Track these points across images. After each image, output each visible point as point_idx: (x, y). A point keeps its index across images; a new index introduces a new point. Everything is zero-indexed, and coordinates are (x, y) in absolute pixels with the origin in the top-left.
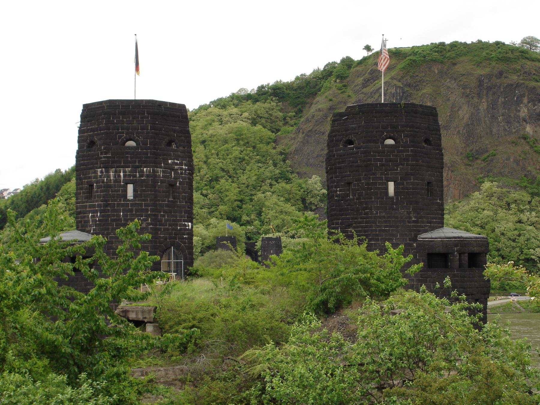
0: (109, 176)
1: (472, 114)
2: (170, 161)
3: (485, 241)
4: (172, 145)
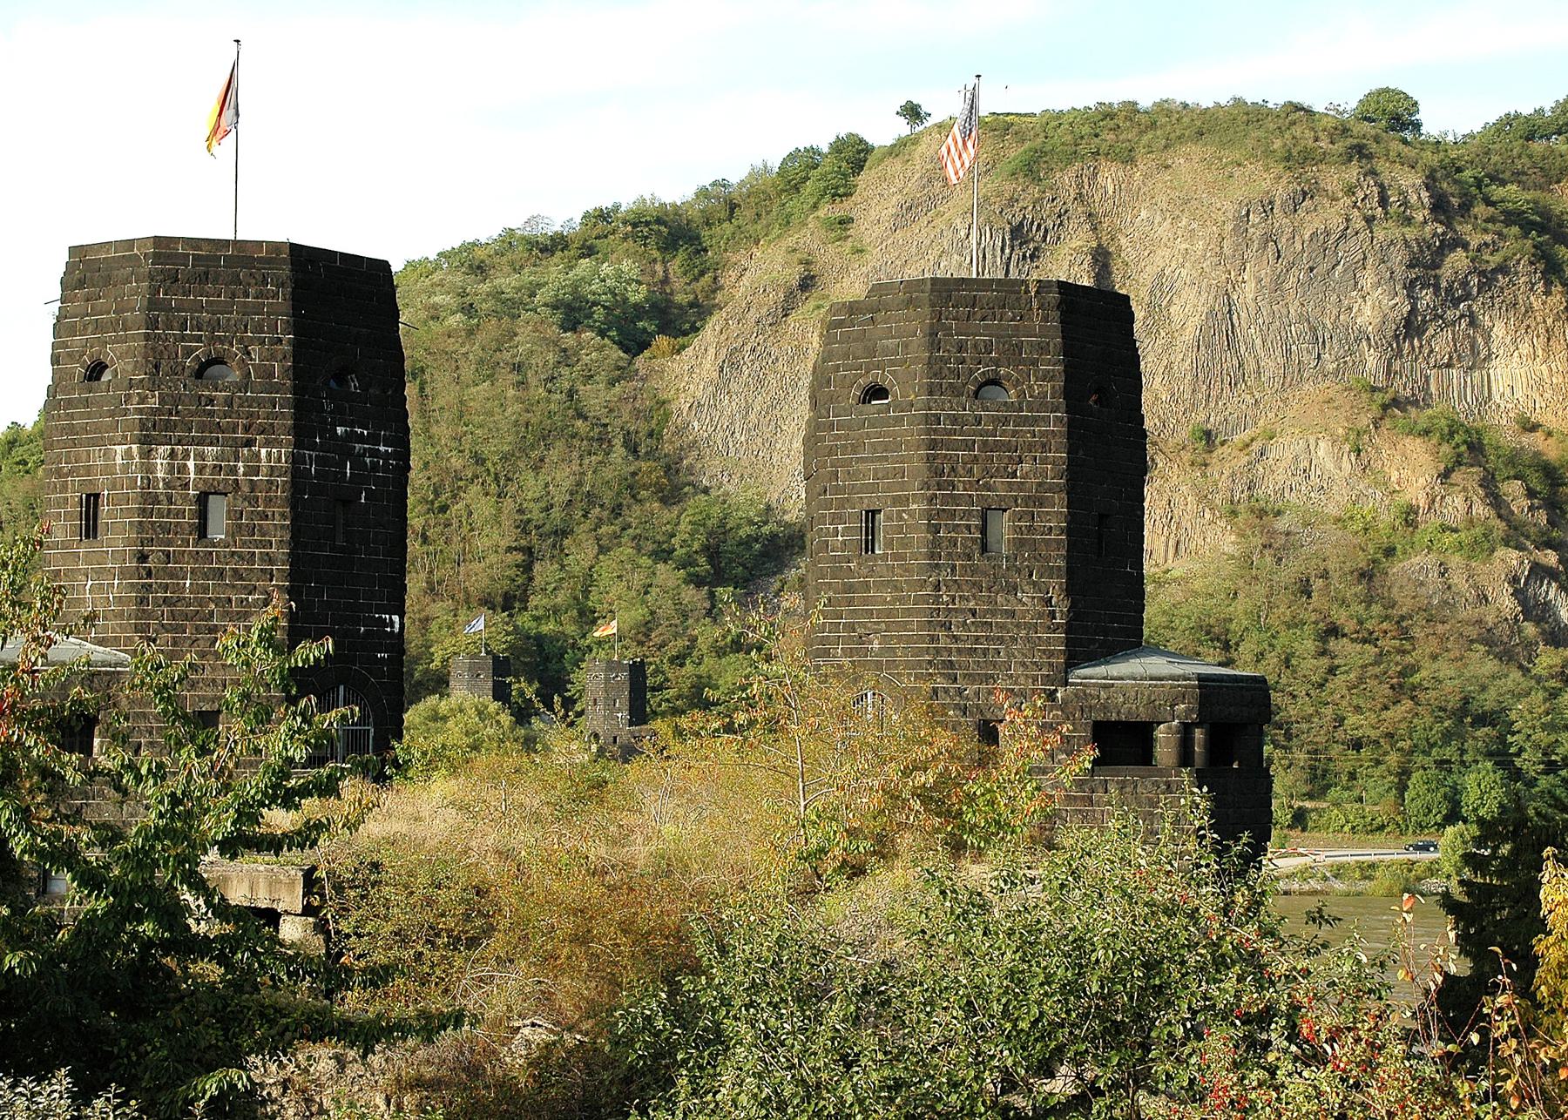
0: (150, 469)
2: (339, 430)
3: (1261, 689)
4: (347, 382)
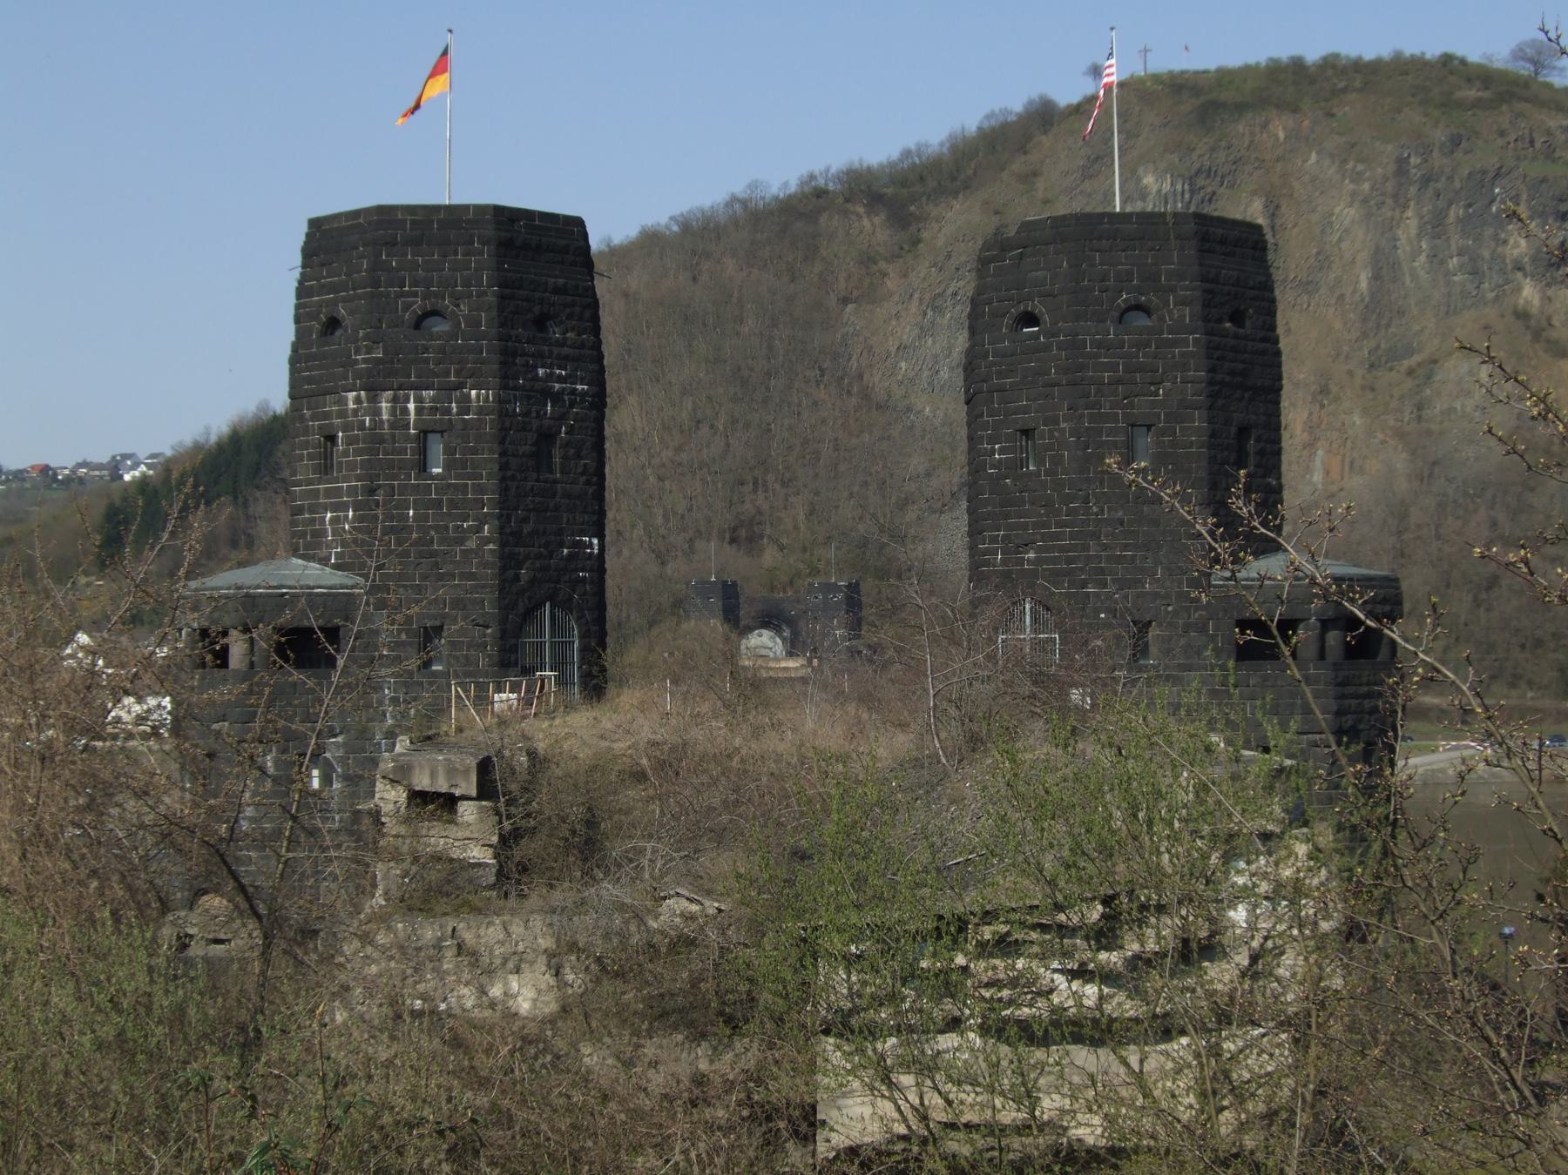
0: (376, 412)
1: (1377, 250)
2: (541, 372)
